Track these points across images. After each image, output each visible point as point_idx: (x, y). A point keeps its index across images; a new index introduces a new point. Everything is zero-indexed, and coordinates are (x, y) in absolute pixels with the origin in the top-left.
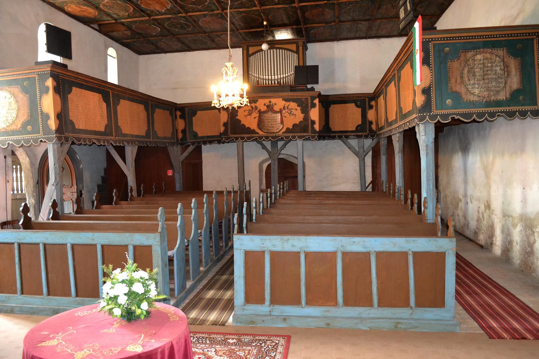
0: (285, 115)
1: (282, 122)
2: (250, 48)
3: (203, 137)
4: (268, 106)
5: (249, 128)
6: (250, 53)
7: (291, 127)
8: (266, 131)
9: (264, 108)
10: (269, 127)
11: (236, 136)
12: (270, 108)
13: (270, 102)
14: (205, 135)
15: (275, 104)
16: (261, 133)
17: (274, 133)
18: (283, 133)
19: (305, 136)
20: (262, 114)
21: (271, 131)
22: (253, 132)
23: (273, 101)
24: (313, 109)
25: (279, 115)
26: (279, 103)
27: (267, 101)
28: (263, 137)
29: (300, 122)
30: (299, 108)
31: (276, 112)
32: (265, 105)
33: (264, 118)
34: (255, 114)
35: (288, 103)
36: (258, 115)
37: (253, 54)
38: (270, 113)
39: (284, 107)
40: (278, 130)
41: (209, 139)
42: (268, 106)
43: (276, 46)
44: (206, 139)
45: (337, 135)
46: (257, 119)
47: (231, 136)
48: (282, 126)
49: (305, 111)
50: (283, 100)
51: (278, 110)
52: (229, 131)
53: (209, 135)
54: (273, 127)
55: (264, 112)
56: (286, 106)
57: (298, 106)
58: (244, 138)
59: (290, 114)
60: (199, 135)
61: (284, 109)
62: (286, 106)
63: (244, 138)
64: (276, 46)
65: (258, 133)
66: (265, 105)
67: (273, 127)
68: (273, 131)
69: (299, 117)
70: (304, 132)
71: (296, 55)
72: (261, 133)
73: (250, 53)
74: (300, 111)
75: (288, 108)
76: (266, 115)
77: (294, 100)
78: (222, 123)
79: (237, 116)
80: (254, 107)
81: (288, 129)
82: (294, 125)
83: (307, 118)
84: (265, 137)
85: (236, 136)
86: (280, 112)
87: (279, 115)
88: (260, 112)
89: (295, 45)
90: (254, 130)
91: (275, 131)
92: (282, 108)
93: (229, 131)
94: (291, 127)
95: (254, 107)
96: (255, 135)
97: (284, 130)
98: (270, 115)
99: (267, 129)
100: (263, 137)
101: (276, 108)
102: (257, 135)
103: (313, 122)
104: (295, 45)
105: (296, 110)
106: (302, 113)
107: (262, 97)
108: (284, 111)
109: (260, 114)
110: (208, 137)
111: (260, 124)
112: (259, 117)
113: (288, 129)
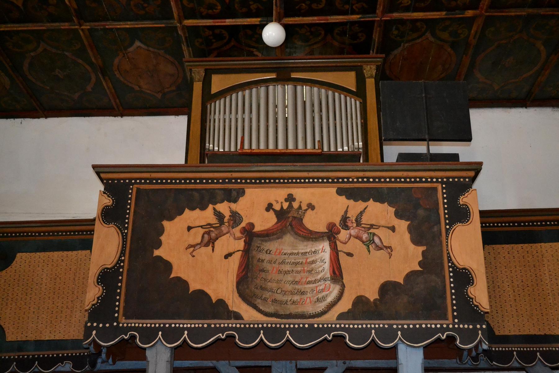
0: (347, 248)
1: (337, 275)
2: (216, 79)
3: (21, 345)
4: (281, 214)
5: (202, 294)
6: (214, 89)
7: (372, 295)
8: (271, 309)
9: (264, 221)
10: (285, 293)
11: (148, 323)
12: (289, 220)
13: (290, 198)
14: (32, 337)
15: (311, 207)
16: (249, 315)
17: (303, 316)
18: (342, 316)
19: (430, 332)
20: (257, 242)
21: (293, 309)
22: (220, 309)
23: (303, 194)
24: (459, 229)
25: (324, 250)
26: (323, 203)
27: (277, 195)
28: (257, 331)
29: (411, 276)
30: (403, 225)
31: (313, 236)
32: (269, 207)
33: (263, 256)
34: (232, 242)
35: (360, 205)
36: (241, 244)
37: (223, 94)
38: (289, 238)
39: (344, 220)
40: (321, 306)
41: (41, 354)
42: (281, 214)
43: (294, 75)
44: (31, 353)
45: (515, 348)
46: (236, 259)
47: (124, 322)
48: (335, 290)
49: (426, 233)
50: (340, 192)
51: (323, 229)
52: (120, 304)
53: (46, 337)
54: (303, 293)
55: (267, 235)
56: (352, 215)
57: (399, 215)
58: (180, 331)
59: (368, 243)
60: (10, 337)
61: (346, 227)
62: (352, 215)
63: (180, 331)
64: (294, 75)
65: (238, 316)
66: (269, 207)
67: (303, 293)
68: (299, 310)
69: (403, 257)
70: (428, 317)
71: (354, 104)
72: (249, 315)
73: (214, 89)
74: (407, 236)
75: (358, 222)
76: (273, 246)
77: (379, 196)
78: (94, 271)
79: (159, 244)
80: (227, 214)
81: (360, 301)
82: (386, 288)
83: (434, 261)
84: (266, 330)
85: (148, 323)
86: (331, 234)
87: (324, 247)
88: (250, 234)
89: (353, 74)
90: (221, 303)
91: (310, 309)
92: (337, 220)
93: (120, 304)
94: (372, 295)
95: (227, 214)
96: (224, 323)
97: (345, 305)
98: (288, 244)
99: (275, 301)
100: (257, 331)
101: (314, 222)
102: (232, 323)
103: (464, 278)
104: (353, 74)
105: (393, 229)
106: (416, 241)
107: (260, 182)
108: (343, 235)
109: (248, 244)
110: (39, 344)
111: (248, 280)
112: (247, 252)
113: (360, 301)
